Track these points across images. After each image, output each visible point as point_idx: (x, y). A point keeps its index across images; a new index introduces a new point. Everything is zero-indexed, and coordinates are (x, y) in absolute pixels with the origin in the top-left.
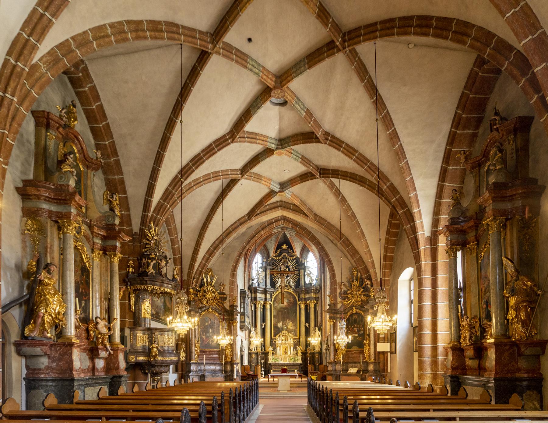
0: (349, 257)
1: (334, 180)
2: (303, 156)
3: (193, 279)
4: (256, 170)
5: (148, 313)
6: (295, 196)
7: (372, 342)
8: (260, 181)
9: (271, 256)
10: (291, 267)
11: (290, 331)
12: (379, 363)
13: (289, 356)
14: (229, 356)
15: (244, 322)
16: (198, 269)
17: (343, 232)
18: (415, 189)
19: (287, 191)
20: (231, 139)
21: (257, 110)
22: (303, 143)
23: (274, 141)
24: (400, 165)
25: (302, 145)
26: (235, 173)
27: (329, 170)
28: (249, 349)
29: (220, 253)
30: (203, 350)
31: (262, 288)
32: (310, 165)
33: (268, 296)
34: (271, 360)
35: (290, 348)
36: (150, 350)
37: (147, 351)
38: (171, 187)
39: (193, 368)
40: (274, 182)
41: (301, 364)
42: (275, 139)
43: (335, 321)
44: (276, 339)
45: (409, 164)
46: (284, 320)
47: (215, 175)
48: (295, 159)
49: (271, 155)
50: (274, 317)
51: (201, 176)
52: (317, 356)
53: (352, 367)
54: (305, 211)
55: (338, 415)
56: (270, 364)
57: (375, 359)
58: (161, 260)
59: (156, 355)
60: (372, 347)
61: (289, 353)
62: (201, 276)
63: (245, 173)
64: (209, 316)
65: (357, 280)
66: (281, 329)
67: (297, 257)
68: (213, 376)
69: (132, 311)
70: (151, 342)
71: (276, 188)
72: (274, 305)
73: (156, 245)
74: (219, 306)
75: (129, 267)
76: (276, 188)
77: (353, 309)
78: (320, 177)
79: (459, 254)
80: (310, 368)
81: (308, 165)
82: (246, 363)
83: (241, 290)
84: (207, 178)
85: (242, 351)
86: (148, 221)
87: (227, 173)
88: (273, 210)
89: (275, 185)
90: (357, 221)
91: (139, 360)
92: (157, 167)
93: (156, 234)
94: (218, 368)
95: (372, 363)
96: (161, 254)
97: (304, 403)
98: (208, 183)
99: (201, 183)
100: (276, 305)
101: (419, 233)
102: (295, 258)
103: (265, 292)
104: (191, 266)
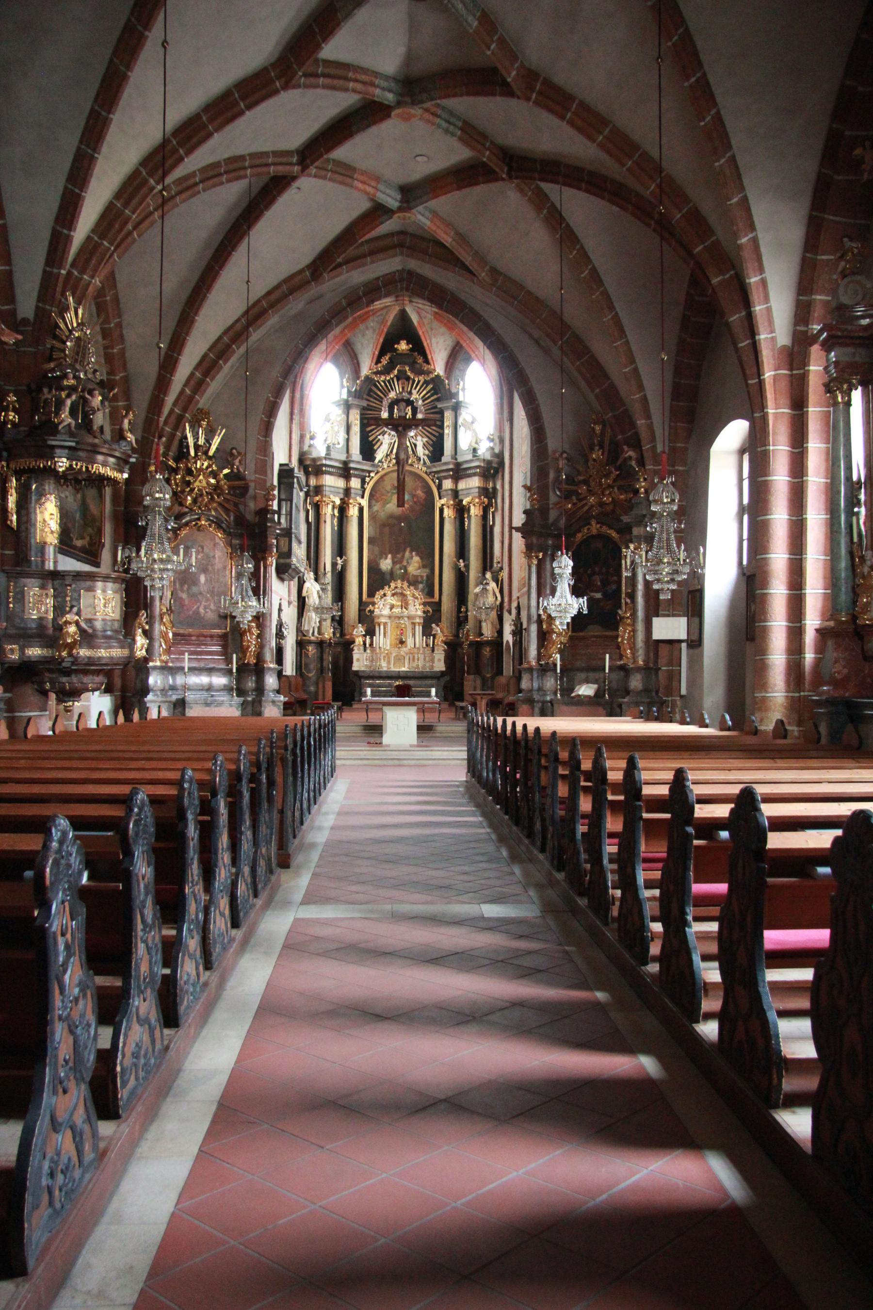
0: (583, 384)
1: (546, 186)
2: (466, 123)
3: (160, 437)
4: (341, 153)
5: (52, 532)
6: (441, 219)
7: (640, 614)
8: (348, 180)
9: (365, 371)
10: (420, 402)
11: (413, 582)
12: (657, 670)
13: (411, 652)
14: (252, 648)
15: (289, 554)
16: (171, 412)
17: (567, 317)
18: (752, 227)
19: (421, 208)
20: (283, 80)
21: (354, 9)
22: (468, 94)
23: (393, 85)
24: (717, 164)
25: (465, 98)
26: (285, 160)
27: (534, 161)
28: (299, 630)
29: (232, 367)
30: (181, 631)
31: (336, 460)
32: (484, 145)
33: (355, 483)
34: (360, 662)
35: (414, 629)
36: (59, 629)
37: (50, 631)
38: (122, 200)
39: (154, 680)
40: (388, 183)
41: (442, 674)
42: (395, 79)
43: (541, 555)
44: (374, 604)
45: (739, 163)
46: (398, 553)
47: (231, 167)
48: (447, 131)
49: (382, 120)
50: (371, 541)
51: (196, 168)
52: (487, 651)
53: (587, 681)
54: (468, 260)
55: (554, 787)
56: (356, 673)
57: (646, 661)
58: (91, 393)
59: (75, 642)
60: (640, 627)
61: (410, 642)
62: (180, 429)
63: (312, 163)
64: (199, 536)
65: (601, 446)
66: (388, 577)
67: (438, 376)
68: (207, 704)
69: (10, 528)
70: (60, 610)
71: (391, 200)
72: (370, 506)
73: (78, 354)
74: (227, 511)
75: (6, 409)
76: (391, 200)
77: (589, 524)
78: (510, 177)
79: (857, 395)
80: (471, 684)
81: (479, 147)
82: (289, 669)
83: (281, 465)
84: (211, 173)
85: (280, 635)
86: (59, 289)
87: (263, 161)
88: (381, 256)
89: (388, 191)
90: (606, 294)
91: (29, 657)
92: (90, 151)
93: (78, 324)
94: (220, 681)
95: (638, 669)
96: (90, 376)
97: (461, 775)
98: (214, 186)
99: (196, 189)
100: (375, 508)
101: (763, 337)
102: (432, 379)
103: (345, 471)
104: (156, 404)
